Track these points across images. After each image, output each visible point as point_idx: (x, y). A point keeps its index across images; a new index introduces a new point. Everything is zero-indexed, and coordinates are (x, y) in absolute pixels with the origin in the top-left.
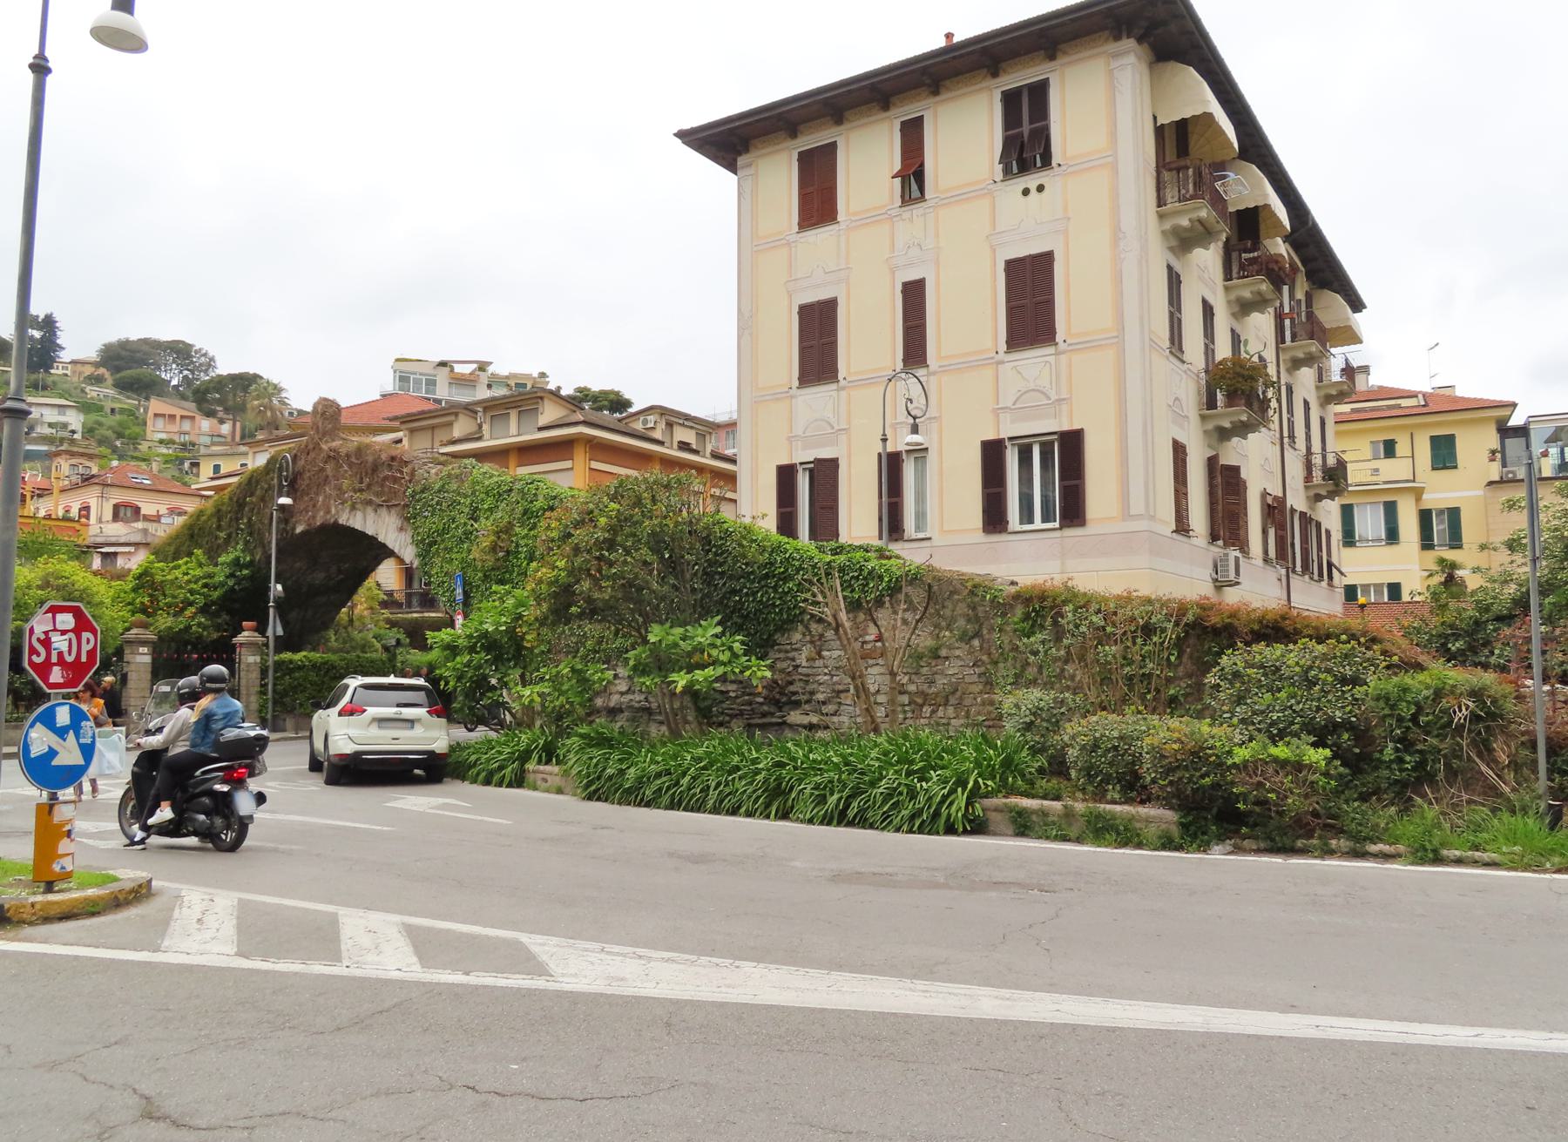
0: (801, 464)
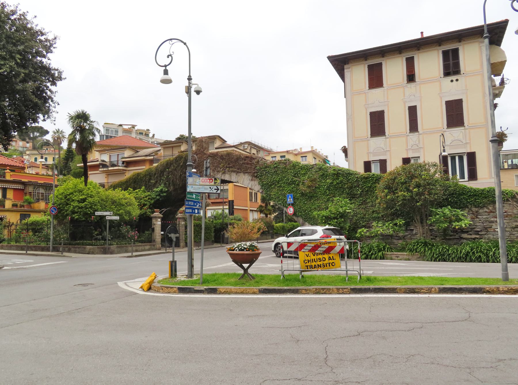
0: (372, 161)
